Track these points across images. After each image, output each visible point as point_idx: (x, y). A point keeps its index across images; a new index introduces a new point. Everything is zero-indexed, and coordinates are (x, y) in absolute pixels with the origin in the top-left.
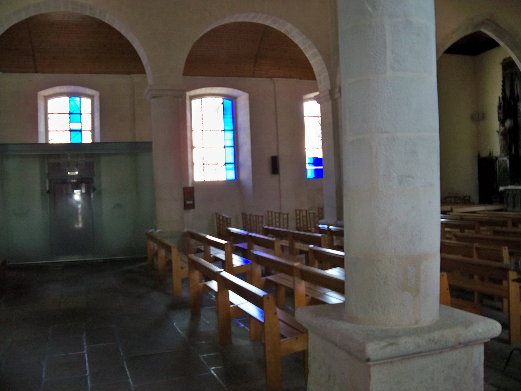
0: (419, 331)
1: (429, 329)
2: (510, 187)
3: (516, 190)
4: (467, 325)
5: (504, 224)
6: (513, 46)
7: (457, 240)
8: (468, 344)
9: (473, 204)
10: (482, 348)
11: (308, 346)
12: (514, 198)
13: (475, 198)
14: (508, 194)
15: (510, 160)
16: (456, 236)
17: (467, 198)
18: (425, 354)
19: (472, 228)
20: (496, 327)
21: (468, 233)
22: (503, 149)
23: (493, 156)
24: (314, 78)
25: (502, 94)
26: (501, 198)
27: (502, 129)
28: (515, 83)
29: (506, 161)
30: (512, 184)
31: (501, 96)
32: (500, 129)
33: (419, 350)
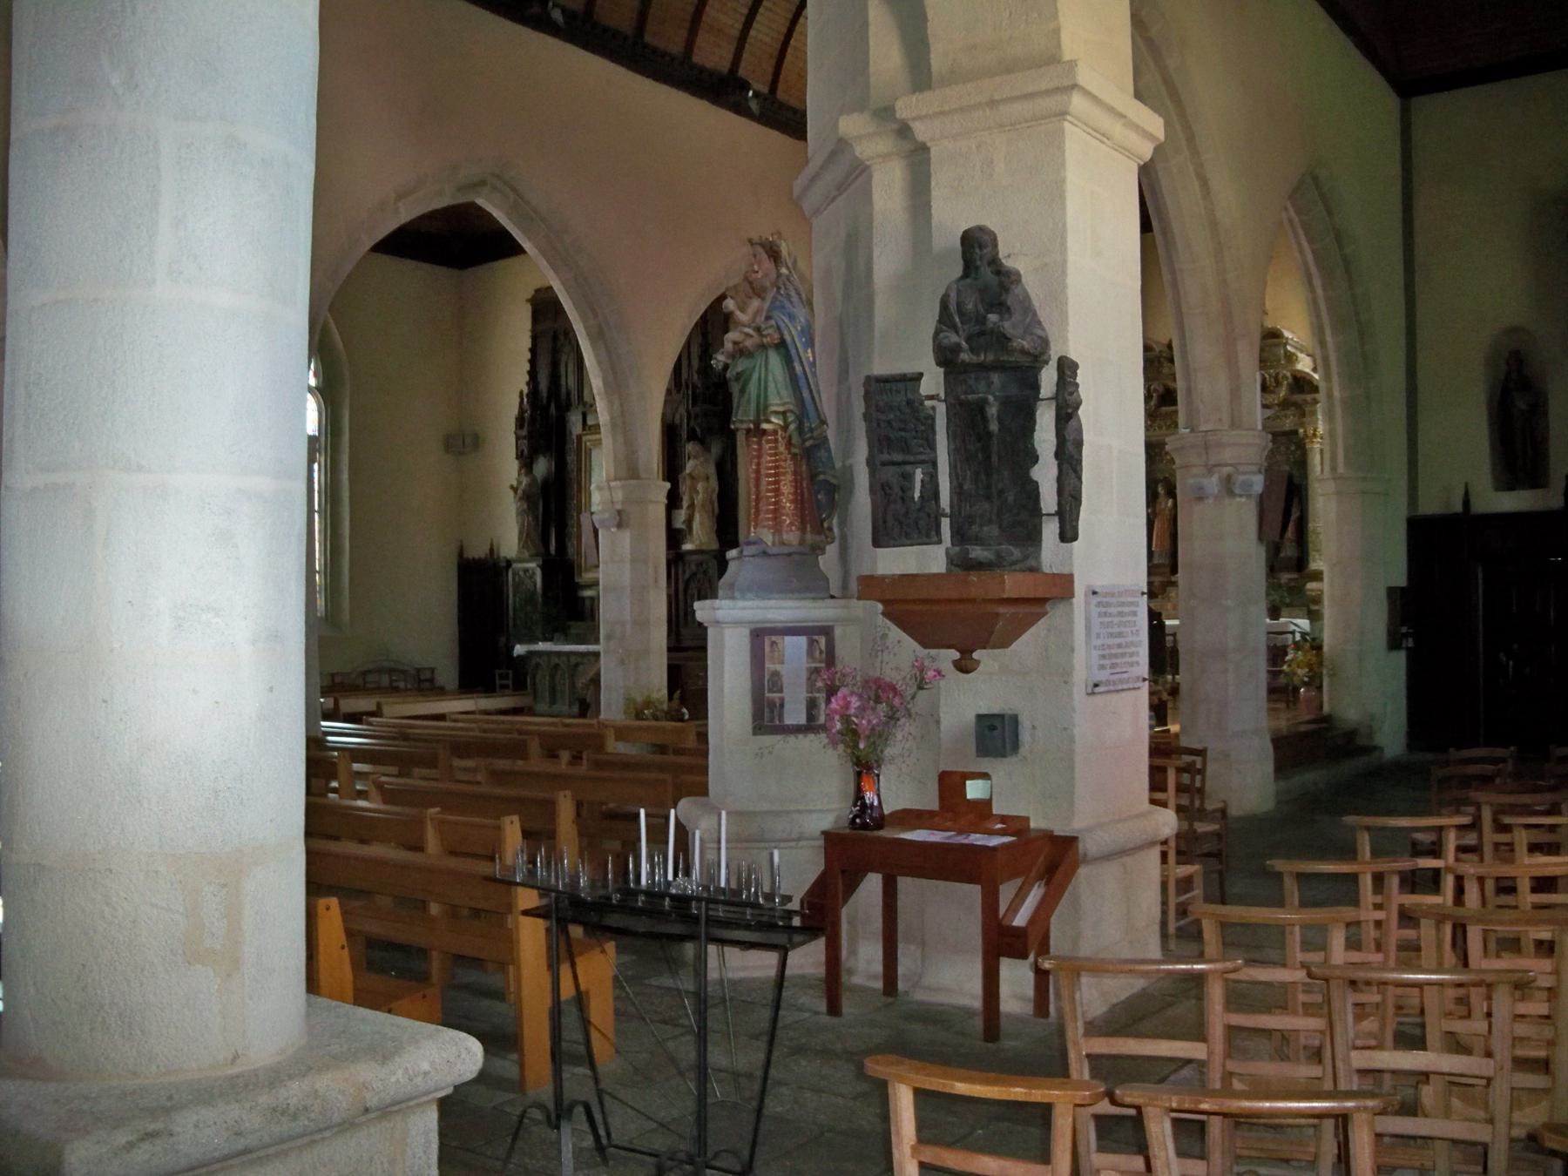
0: (237, 1087)
1: (275, 1076)
2: (541, 646)
3: (559, 654)
4: (383, 1052)
5: (517, 750)
6: (559, 258)
7: (385, 802)
8: (392, 1109)
9: (440, 692)
10: (432, 1116)
11: (1177, 778)
12: (552, 677)
13: (448, 674)
14: (538, 665)
15: (544, 568)
16: (380, 787)
17: (427, 675)
18: (262, 1153)
19: (431, 762)
20: (468, 1050)
21: (418, 779)
22: (525, 537)
23: (499, 557)
24: (805, 139)
25: (528, 384)
26: (519, 675)
27: (525, 481)
28: (564, 358)
29: (533, 569)
30: (545, 640)
31: (526, 391)
32: (520, 483)
33: (241, 1144)
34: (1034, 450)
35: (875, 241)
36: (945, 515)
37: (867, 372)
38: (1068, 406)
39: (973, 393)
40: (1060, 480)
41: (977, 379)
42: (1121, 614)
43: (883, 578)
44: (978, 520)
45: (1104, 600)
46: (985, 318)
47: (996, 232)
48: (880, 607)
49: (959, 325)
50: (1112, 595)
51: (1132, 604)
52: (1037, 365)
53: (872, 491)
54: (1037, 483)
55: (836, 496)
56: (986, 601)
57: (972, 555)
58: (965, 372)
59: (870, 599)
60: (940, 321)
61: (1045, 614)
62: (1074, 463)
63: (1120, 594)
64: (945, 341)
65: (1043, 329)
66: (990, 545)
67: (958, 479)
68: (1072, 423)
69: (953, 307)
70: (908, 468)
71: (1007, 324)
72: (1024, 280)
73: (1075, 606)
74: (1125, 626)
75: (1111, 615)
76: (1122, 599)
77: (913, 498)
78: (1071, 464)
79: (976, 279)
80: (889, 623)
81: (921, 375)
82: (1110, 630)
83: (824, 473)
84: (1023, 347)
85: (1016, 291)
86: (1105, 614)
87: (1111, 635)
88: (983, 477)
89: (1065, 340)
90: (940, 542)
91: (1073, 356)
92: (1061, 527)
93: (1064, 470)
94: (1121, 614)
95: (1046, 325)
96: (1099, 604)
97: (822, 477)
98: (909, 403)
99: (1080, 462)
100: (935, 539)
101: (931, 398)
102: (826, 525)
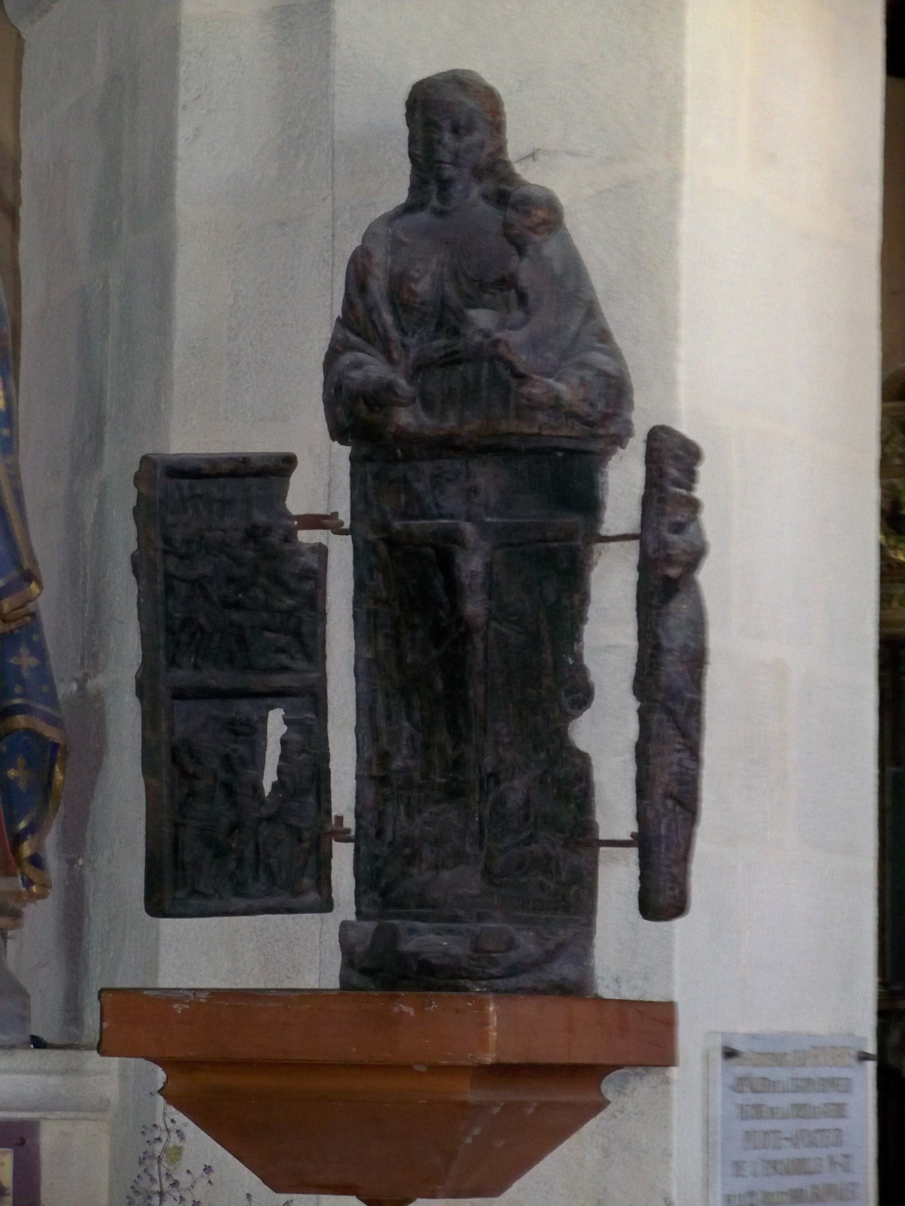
34: (581, 670)
35: (184, 97)
36: (343, 836)
37: (148, 450)
38: (669, 560)
39: (425, 516)
40: (642, 753)
41: (437, 480)
42: (801, 1111)
43: (170, 996)
44: (427, 853)
45: (758, 1072)
46: (463, 320)
47: (501, 90)
48: (161, 1076)
49: (395, 335)
50: (778, 1059)
51: (831, 1084)
52: (598, 446)
53: (149, 767)
54: (585, 758)
55: (59, 776)
56: (435, 1069)
57: (409, 945)
58: (408, 458)
59: (135, 1056)
60: (346, 322)
61: (600, 1105)
62: (680, 709)
63: (802, 1058)
64: (356, 374)
65: (615, 354)
66: (455, 919)
67: (376, 739)
68: (680, 607)
69: (378, 285)
70: (245, 707)
71: (516, 338)
72: (569, 221)
73: (675, 1090)
74: (813, 1144)
75: (773, 1113)
76: (804, 1072)
77: (257, 787)
78: (671, 713)
79: (441, 214)
80: (181, 1119)
81: (288, 463)
82: (773, 1155)
83: (24, 710)
84: (558, 398)
85: (547, 251)
86: (758, 1111)
87: (773, 1167)
88: (443, 737)
89: (670, 382)
90: (326, 905)
91: (685, 428)
92: (643, 878)
93: (654, 727)
94: (801, 1111)
95: (622, 340)
96: (741, 1084)
97: (21, 721)
98: (254, 535)
99: (695, 708)
100: (313, 897)
101: (314, 522)
102: (26, 850)
